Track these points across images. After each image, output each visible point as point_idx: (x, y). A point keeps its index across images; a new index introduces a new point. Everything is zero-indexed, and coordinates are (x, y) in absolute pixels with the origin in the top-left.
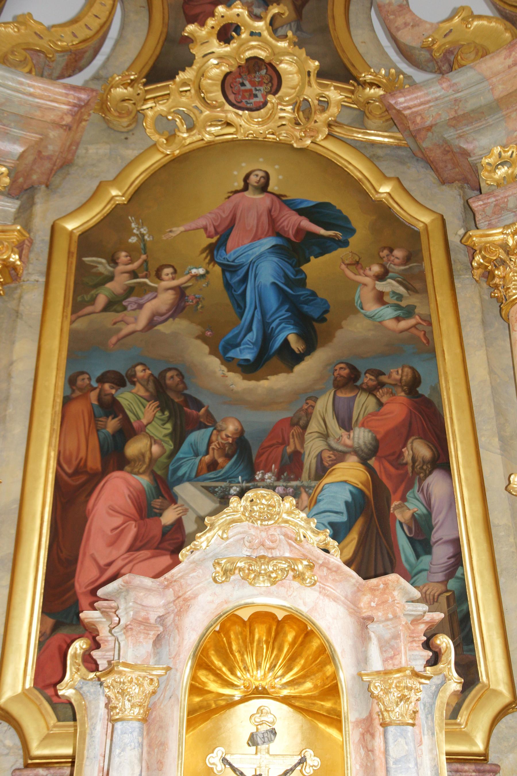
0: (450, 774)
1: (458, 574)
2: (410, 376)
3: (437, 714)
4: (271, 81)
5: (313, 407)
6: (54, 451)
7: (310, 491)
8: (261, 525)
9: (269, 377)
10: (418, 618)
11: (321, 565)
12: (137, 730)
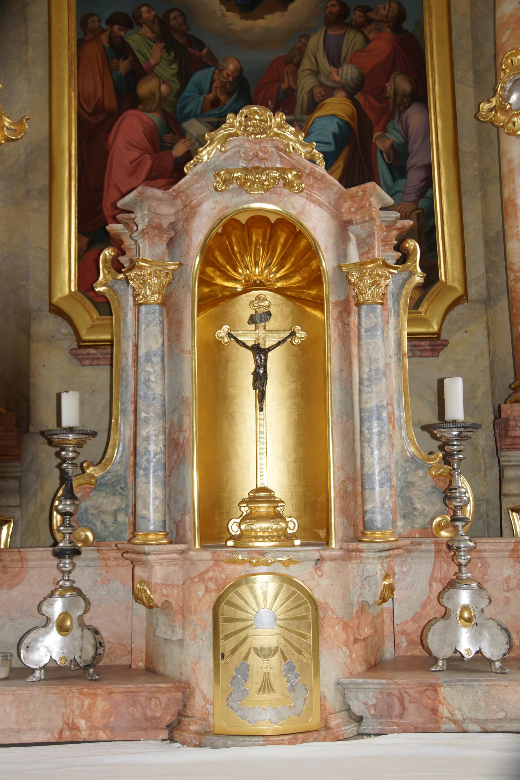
0: (410, 348)
1: (428, 194)
3: (402, 305)
5: (306, 45)
6: (74, 91)
7: (303, 124)
8: (255, 138)
9: (265, 16)
10: (392, 224)
11: (308, 175)
12: (158, 311)
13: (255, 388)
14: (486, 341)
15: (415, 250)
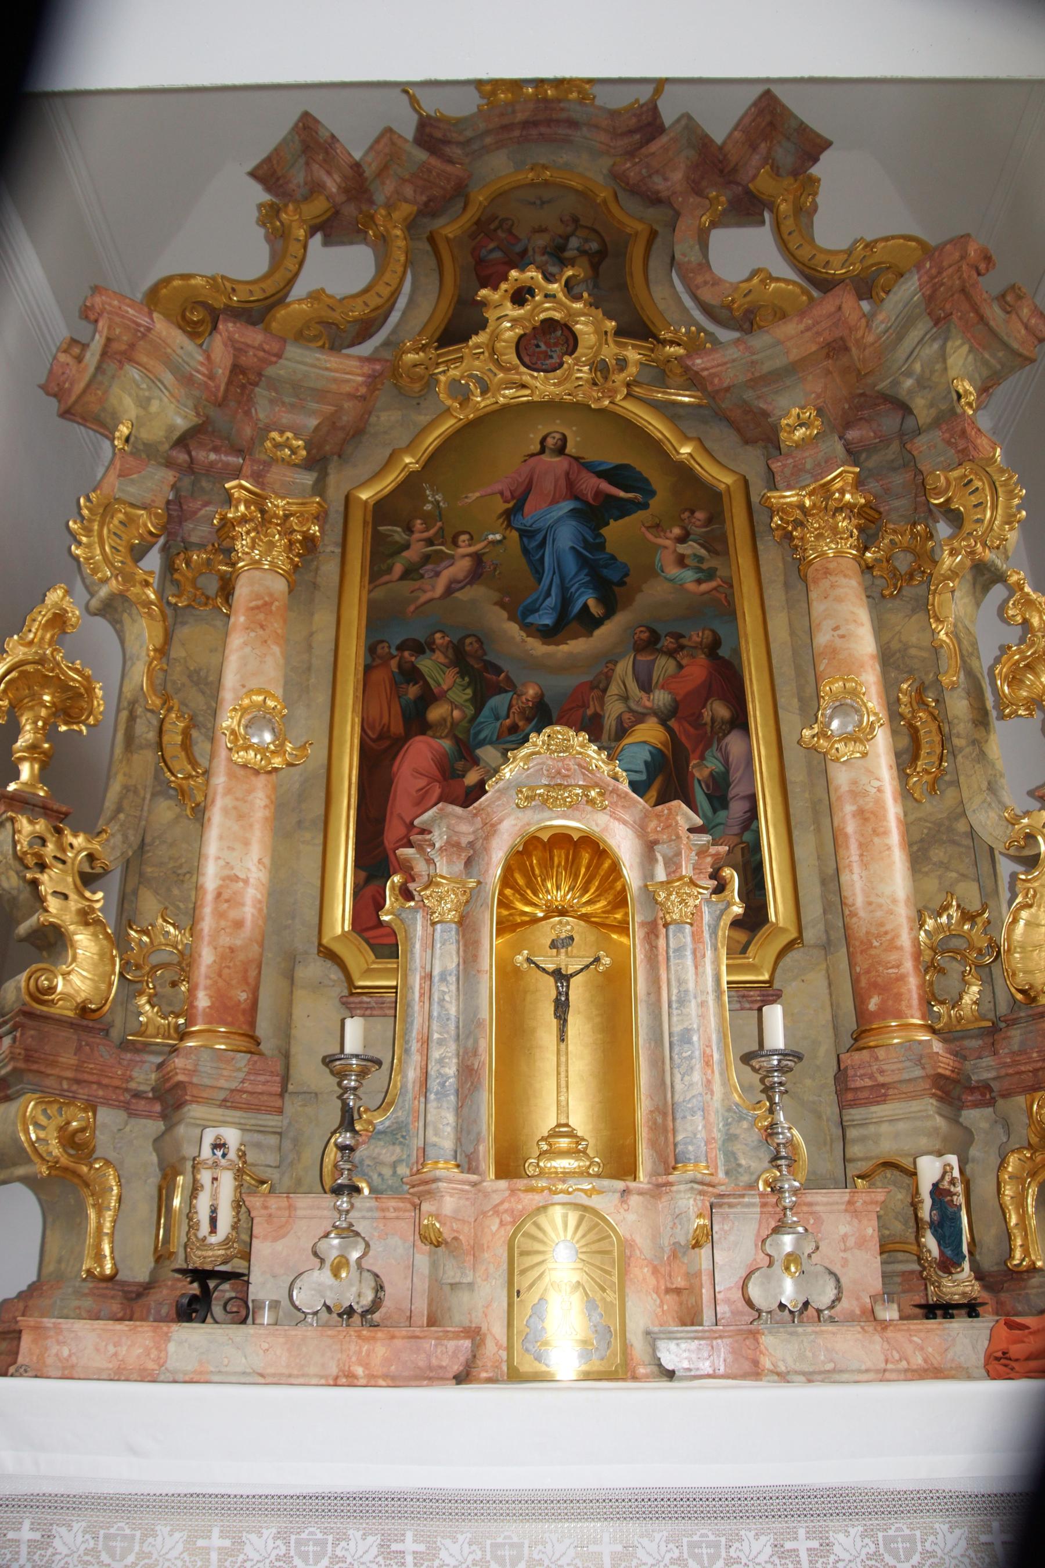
1: (753, 826)
2: (710, 638)
4: (567, 342)
13: (556, 1017)
14: (827, 991)
15: (732, 876)
